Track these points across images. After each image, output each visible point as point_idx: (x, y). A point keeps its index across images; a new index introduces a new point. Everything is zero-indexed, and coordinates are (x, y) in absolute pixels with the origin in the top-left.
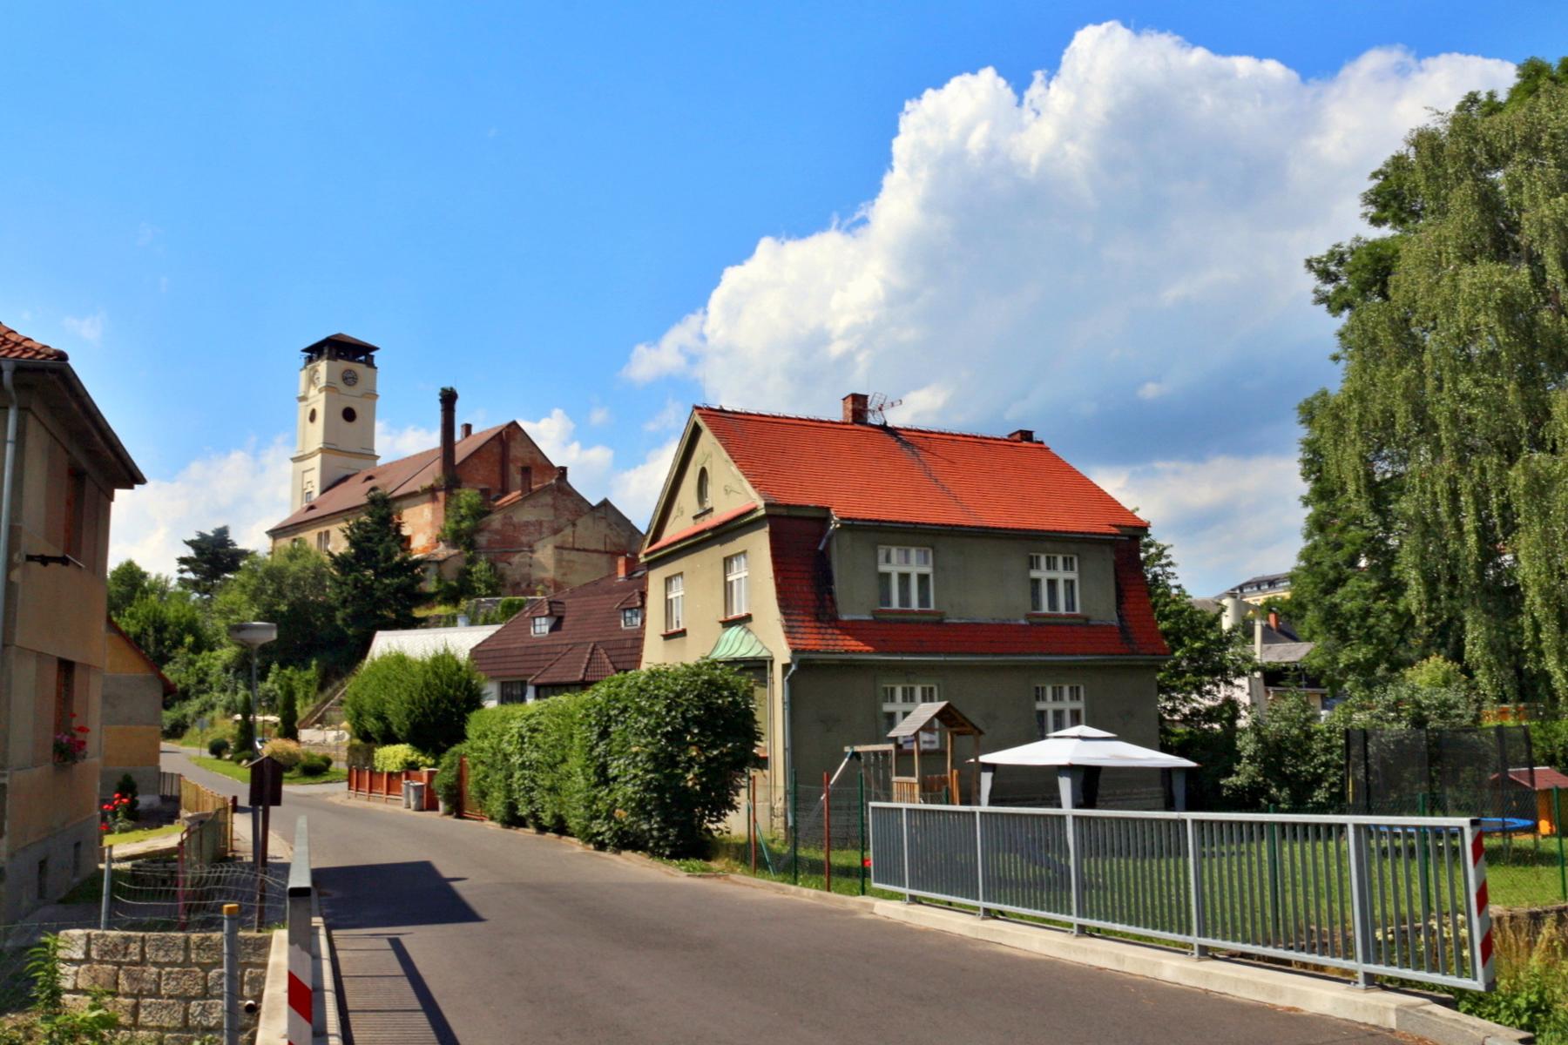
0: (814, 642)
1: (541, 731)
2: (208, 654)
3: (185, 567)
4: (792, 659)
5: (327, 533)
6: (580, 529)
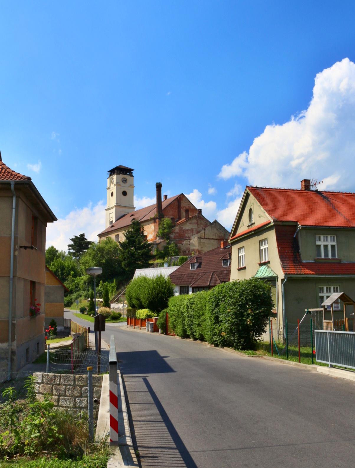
0: (293, 271)
1: (195, 304)
2: (79, 278)
3: (70, 248)
5: (118, 235)
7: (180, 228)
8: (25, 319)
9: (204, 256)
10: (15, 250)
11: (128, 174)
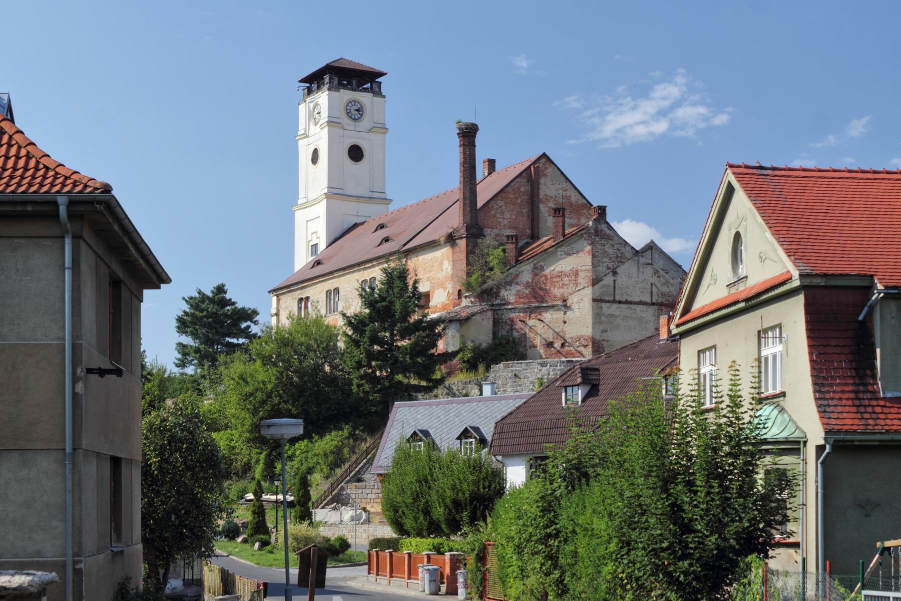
0: (850, 422)
4: (826, 439)
5: (337, 290)
6: (622, 280)
7: (535, 268)
8: (101, 557)
9: (607, 363)
10: (75, 380)
11: (365, 86)
